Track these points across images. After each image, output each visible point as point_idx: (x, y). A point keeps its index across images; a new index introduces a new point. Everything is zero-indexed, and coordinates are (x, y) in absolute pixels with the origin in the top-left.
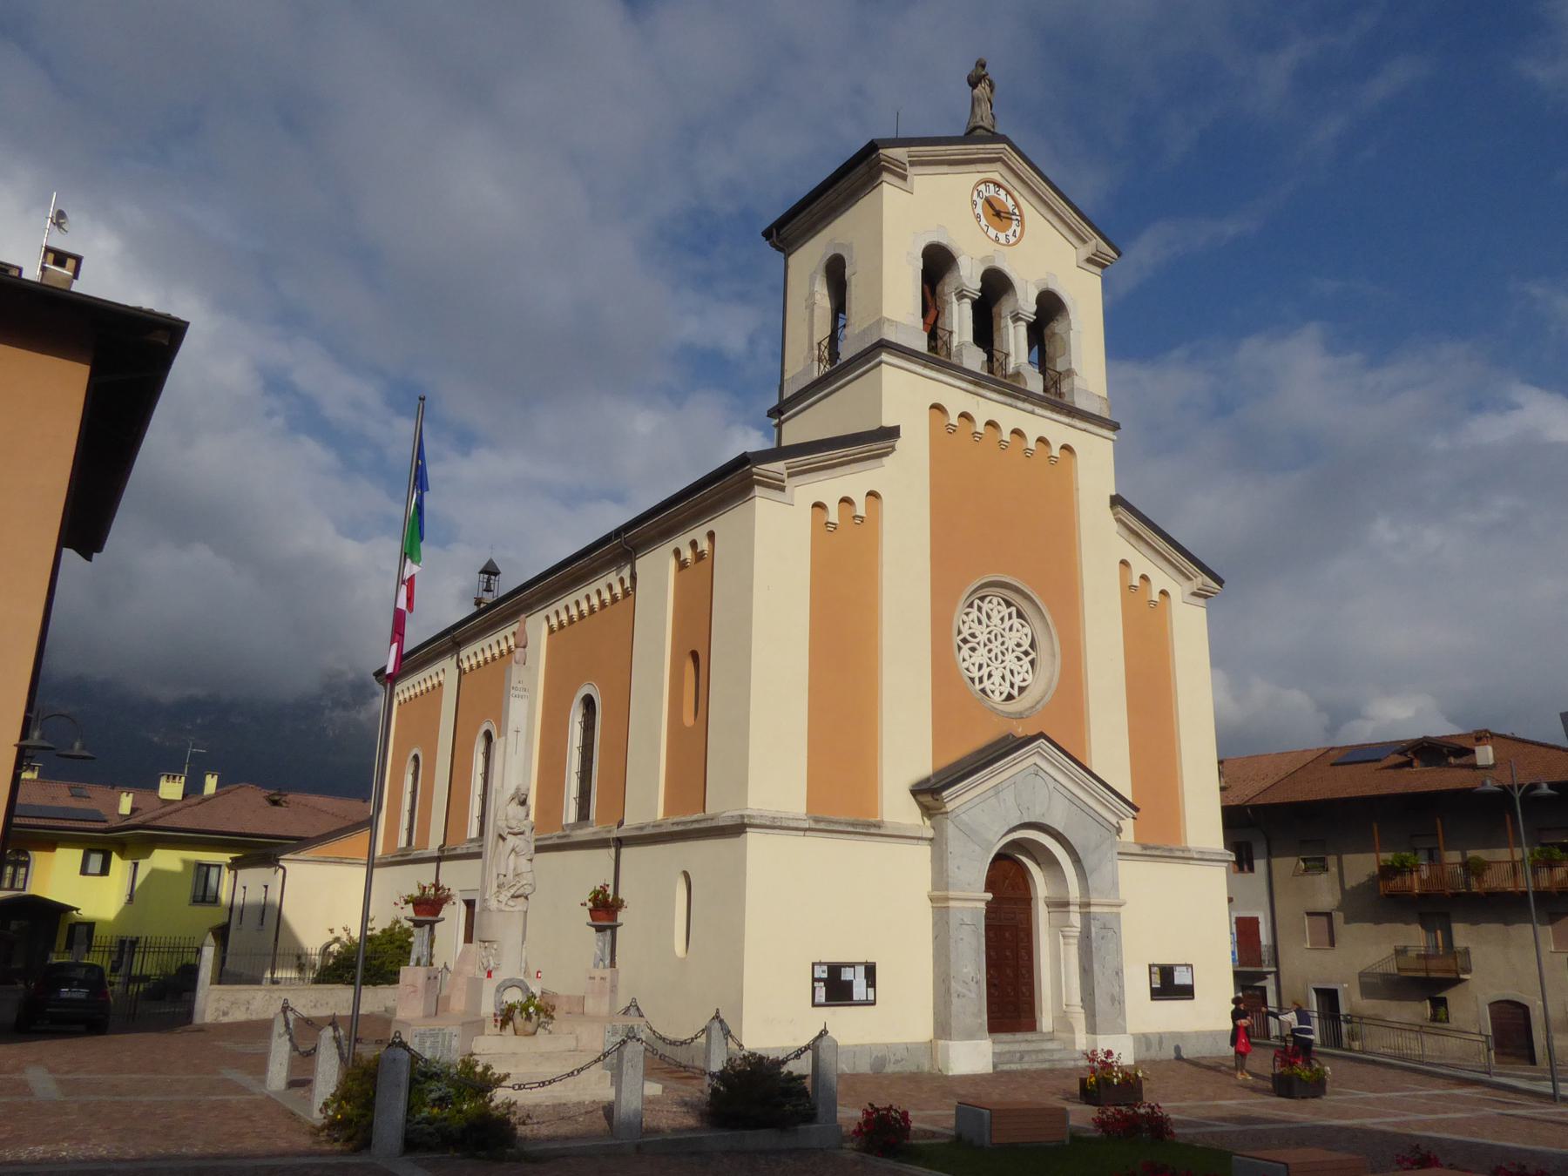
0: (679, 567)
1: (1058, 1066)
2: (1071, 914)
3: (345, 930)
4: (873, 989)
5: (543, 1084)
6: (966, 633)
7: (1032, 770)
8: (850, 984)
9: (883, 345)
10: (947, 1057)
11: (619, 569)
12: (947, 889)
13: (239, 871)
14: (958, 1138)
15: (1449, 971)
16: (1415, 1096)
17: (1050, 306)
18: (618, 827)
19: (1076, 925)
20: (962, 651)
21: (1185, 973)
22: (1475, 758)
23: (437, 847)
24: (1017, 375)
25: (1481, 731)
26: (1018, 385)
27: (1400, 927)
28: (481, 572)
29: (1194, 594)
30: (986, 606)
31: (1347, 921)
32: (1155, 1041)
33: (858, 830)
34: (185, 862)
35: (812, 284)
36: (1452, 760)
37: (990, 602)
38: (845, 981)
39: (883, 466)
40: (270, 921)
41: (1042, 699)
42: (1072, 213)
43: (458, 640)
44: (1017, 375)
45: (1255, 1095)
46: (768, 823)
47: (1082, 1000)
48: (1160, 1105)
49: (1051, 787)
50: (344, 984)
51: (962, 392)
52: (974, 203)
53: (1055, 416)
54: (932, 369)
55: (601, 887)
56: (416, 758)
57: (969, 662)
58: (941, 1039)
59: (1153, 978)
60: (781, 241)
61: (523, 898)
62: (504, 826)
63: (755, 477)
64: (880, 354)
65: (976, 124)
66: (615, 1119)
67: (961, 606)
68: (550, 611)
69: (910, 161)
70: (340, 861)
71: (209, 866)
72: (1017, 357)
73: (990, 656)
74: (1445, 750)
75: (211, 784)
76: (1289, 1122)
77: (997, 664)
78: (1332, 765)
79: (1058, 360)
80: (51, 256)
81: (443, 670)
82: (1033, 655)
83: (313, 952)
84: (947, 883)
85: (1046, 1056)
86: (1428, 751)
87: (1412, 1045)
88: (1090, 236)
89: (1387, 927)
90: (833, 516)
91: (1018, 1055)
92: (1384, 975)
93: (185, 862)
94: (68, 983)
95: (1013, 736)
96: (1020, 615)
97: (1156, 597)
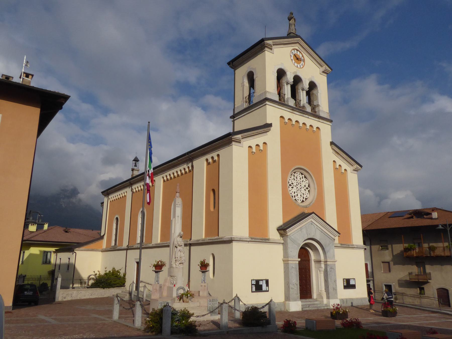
0: (208, 164)
1: (319, 308)
2: (322, 264)
3: (98, 272)
4: (268, 287)
5: (203, 316)
6: (290, 183)
7: (310, 223)
9: (267, 99)
10: (289, 306)
11: (188, 164)
12: (288, 258)
13: (58, 254)
14: (307, 328)
15: (425, 279)
16: (420, 316)
17: (312, 85)
18: (190, 240)
19: (323, 267)
20: (290, 188)
22: (432, 216)
23: (126, 246)
24: (304, 107)
25: (434, 208)
26: (304, 110)
27: (410, 266)
28: (133, 161)
29: (354, 170)
30: (296, 175)
31: (394, 264)
32: (345, 301)
34: (40, 251)
35: (243, 80)
36: (425, 216)
37: (297, 174)
38: (260, 285)
39: (267, 135)
40: (71, 269)
41: (312, 202)
42: (318, 58)
43: (131, 183)
44: (304, 107)
45: (376, 316)
46: (239, 240)
47: (325, 289)
48: (358, 319)
49: (316, 228)
50: (100, 288)
51: (289, 112)
52: (291, 56)
54: (280, 106)
55: (203, 260)
56: (117, 219)
57: (292, 191)
58: (287, 301)
59: (344, 282)
60: (233, 66)
61: (182, 264)
62: (177, 244)
63: (233, 139)
64: (265, 102)
65: (291, 32)
66: (221, 326)
67: (289, 175)
68: (164, 175)
69: (273, 44)
70: (92, 250)
71: (47, 252)
72: (303, 101)
73: (297, 189)
74: (423, 213)
75: (46, 227)
76: (390, 323)
77: (299, 192)
78: (389, 217)
79: (314, 102)
80: (25, 75)
81: (126, 192)
82: (309, 189)
83: (85, 279)
84: (288, 256)
85: (316, 306)
86: (418, 214)
87: (417, 302)
89: (406, 266)
90: (254, 150)
91: (308, 306)
92: (406, 280)
93: (40, 251)
94: (27, 290)
95: (304, 213)
96: (305, 177)
97: (343, 171)
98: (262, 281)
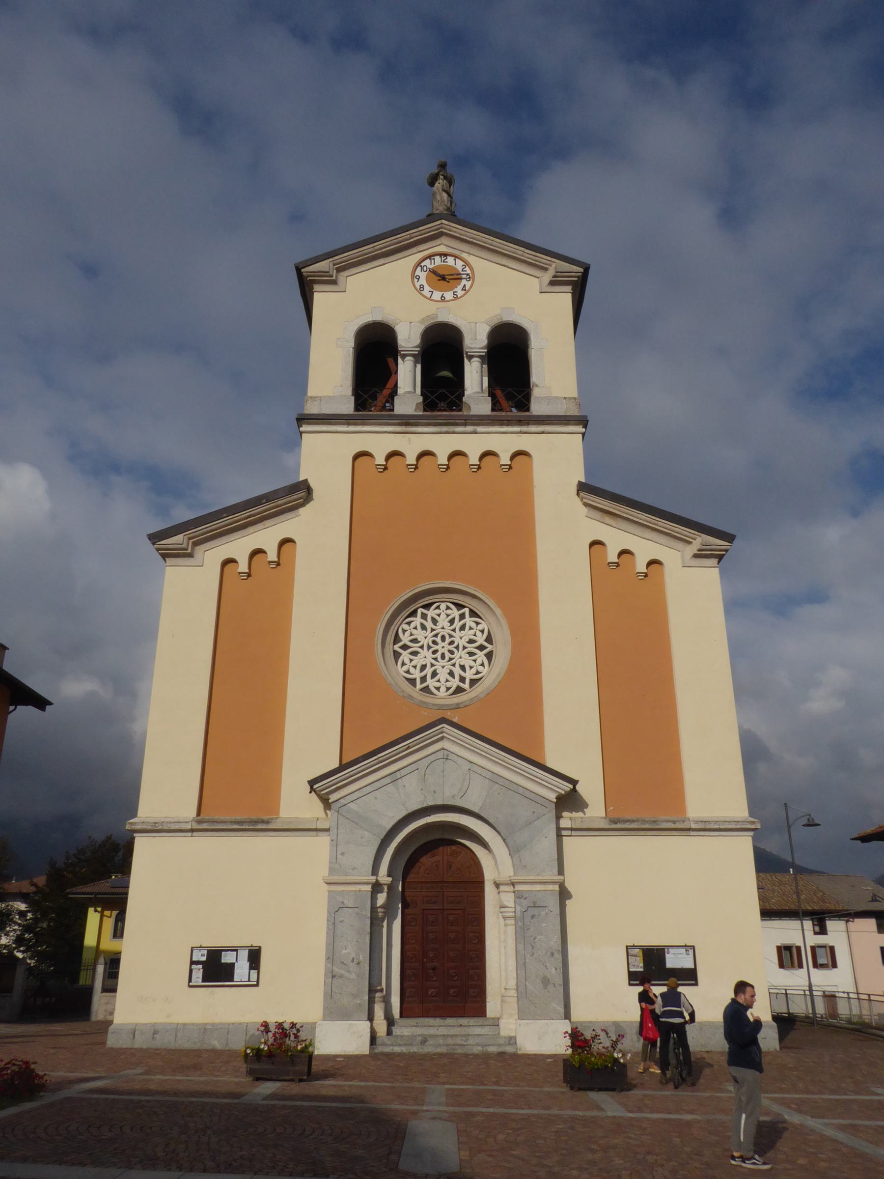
8: (231, 967)
21: (684, 955)
29: (696, 556)
33: (244, 827)
39: (300, 515)
46: (149, 828)
53: (505, 429)
88: (549, 262)
96: (473, 614)
98: (236, 950)
